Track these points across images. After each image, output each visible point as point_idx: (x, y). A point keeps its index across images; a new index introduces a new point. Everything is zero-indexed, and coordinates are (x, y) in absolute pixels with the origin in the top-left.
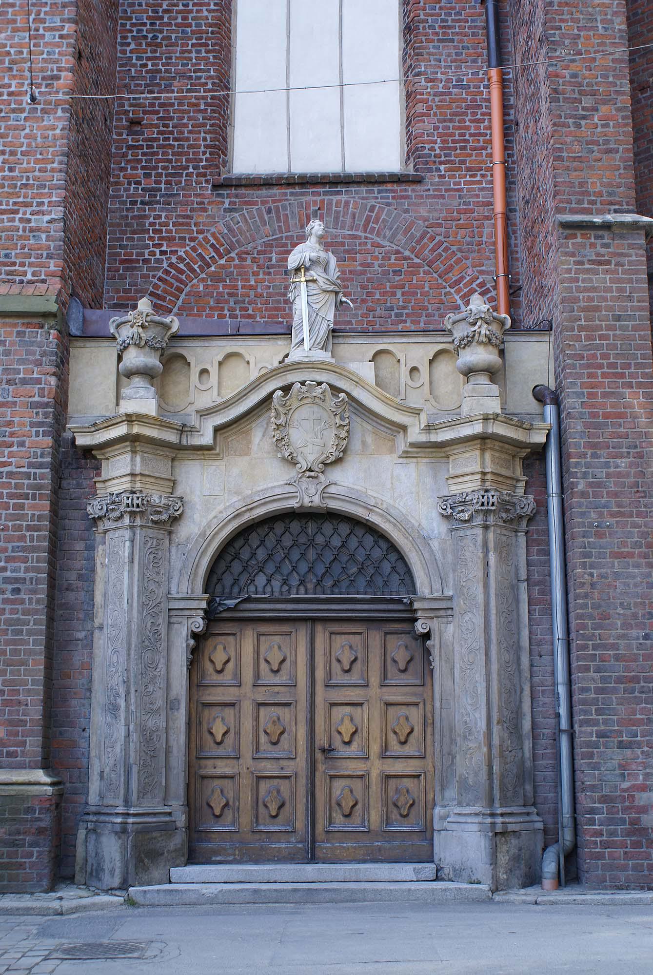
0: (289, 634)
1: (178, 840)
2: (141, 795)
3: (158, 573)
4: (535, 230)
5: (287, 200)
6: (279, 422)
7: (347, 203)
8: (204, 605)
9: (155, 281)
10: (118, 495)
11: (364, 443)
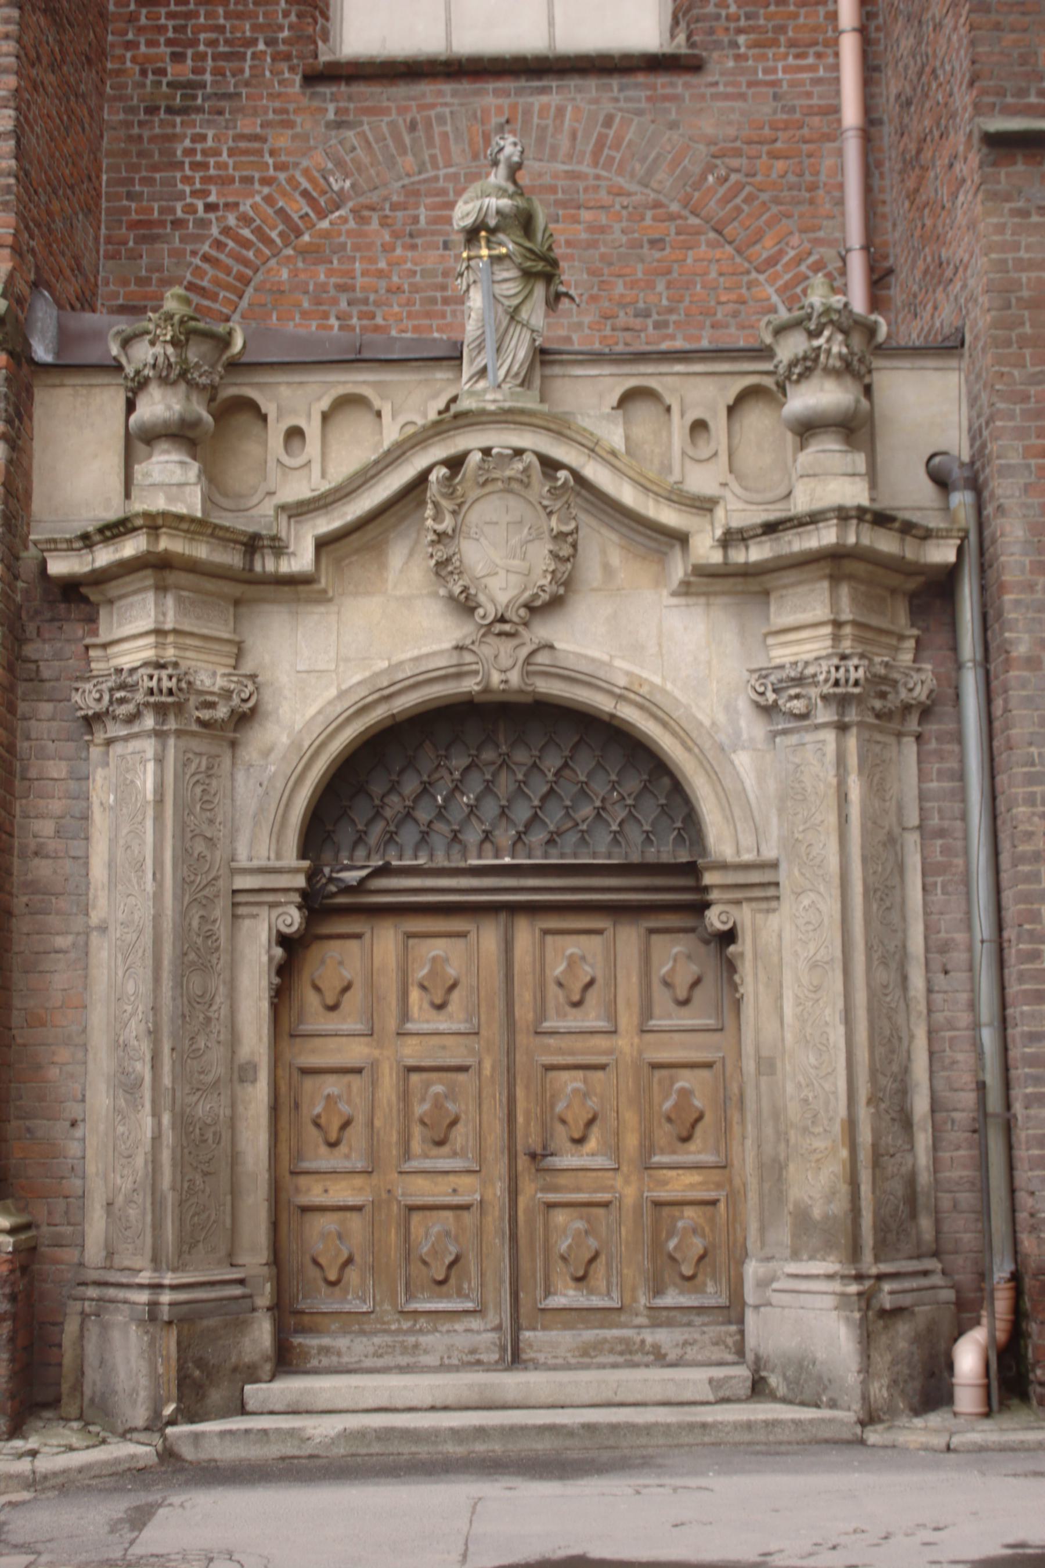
0: (463, 935)
1: (261, 1335)
2: (185, 1248)
3: (211, 821)
4: (927, 155)
5: (446, 104)
6: (440, 528)
7: (560, 111)
8: (300, 881)
9: (197, 261)
10: (133, 671)
11: (607, 568)
